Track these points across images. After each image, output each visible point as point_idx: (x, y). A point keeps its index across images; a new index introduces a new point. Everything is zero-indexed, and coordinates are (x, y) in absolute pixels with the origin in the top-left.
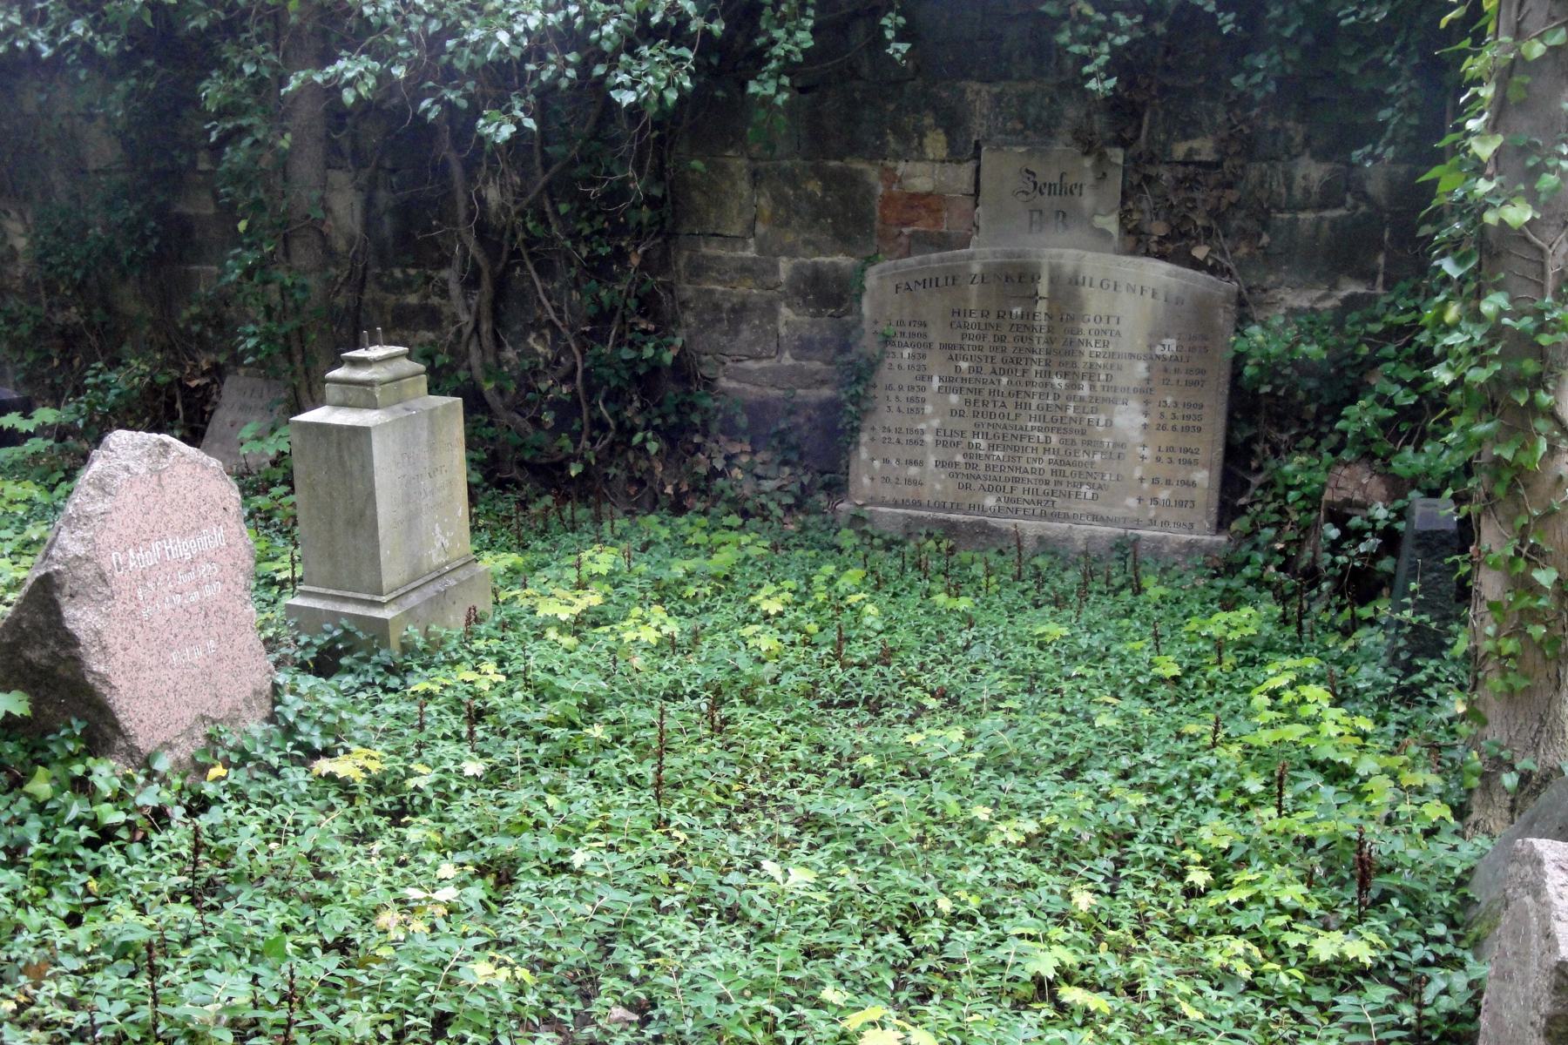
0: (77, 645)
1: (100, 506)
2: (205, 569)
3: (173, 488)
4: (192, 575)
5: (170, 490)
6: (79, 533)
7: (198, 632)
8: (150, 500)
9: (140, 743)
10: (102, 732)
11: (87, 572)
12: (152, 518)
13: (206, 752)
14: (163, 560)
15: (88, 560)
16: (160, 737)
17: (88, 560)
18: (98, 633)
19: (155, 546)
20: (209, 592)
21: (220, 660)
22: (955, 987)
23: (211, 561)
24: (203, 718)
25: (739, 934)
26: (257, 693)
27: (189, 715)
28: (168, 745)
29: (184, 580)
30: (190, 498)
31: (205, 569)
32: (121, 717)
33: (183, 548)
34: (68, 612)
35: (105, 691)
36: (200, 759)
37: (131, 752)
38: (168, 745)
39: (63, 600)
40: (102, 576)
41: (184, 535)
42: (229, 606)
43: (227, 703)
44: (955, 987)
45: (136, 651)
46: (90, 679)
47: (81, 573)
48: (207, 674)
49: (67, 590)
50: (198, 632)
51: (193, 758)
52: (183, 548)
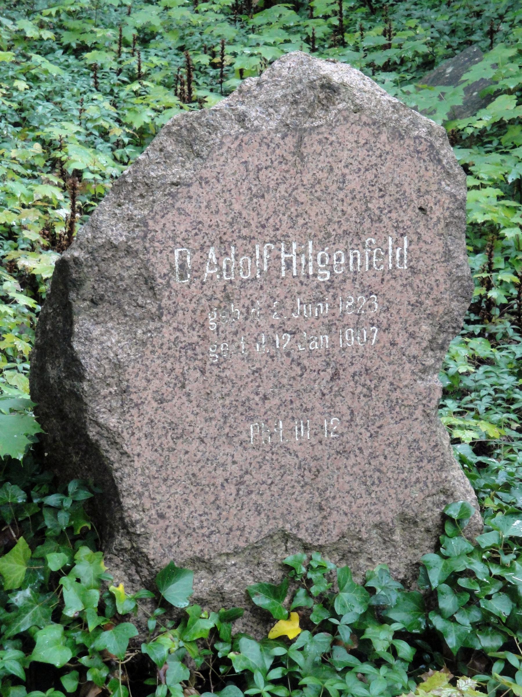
0: (81, 378)
1: (176, 172)
2: (351, 301)
3: (323, 161)
4: (324, 308)
5: (314, 168)
6: (128, 208)
7: (311, 400)
8: (270, 177)
9: (152, 549)
10: (102, 521)
11: (124, 270)
12: (267, 205)
13: (275, 591)
14: (271, 276)
15: (129, 251)
16: (189, 548)
17: (129, 251)
18: (118, 366)
19: (262, 251)
20: (350, 339)
21: (343, 452)
22: (364, 375)
23: (368, 291)
24: (286, 537)
25: (115, 23)
26: (408, 521)
27: (256, 526)
28: (200, 563)
29: (303, 311)
30: (354, 182)
31: (351, 301)
32: (127, 502)
33: (314, 261)
34: (82, 324)
35: (113, 456)
36: (262, 601)
37: (137, 559)
38: (200, 563)
39: (80, 305)
40: (149, 282)
41: (325, 240)
42: (387, 370)
43: (337, 524)
44: (364, 375)
45: (181, 408)
46: (92, 432)
47: (114, 269)
48: (311, 472)
49: (87, 290)
50: (311, 400)
51: (248, 596)
52: (314, 261)
